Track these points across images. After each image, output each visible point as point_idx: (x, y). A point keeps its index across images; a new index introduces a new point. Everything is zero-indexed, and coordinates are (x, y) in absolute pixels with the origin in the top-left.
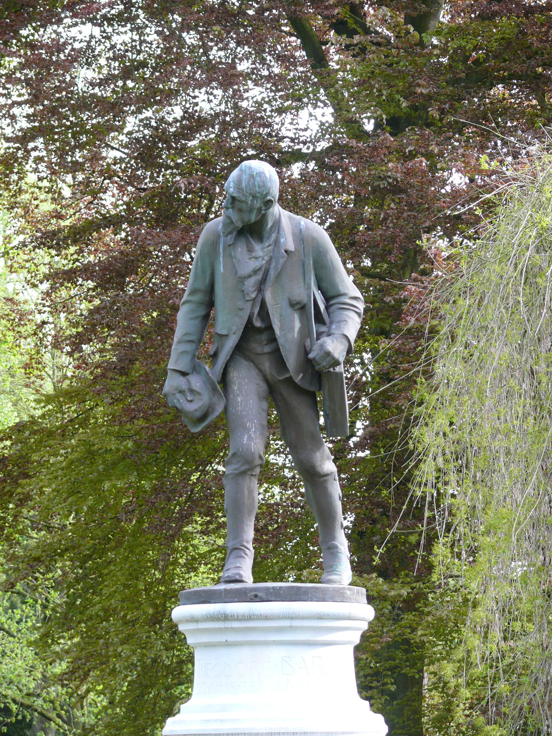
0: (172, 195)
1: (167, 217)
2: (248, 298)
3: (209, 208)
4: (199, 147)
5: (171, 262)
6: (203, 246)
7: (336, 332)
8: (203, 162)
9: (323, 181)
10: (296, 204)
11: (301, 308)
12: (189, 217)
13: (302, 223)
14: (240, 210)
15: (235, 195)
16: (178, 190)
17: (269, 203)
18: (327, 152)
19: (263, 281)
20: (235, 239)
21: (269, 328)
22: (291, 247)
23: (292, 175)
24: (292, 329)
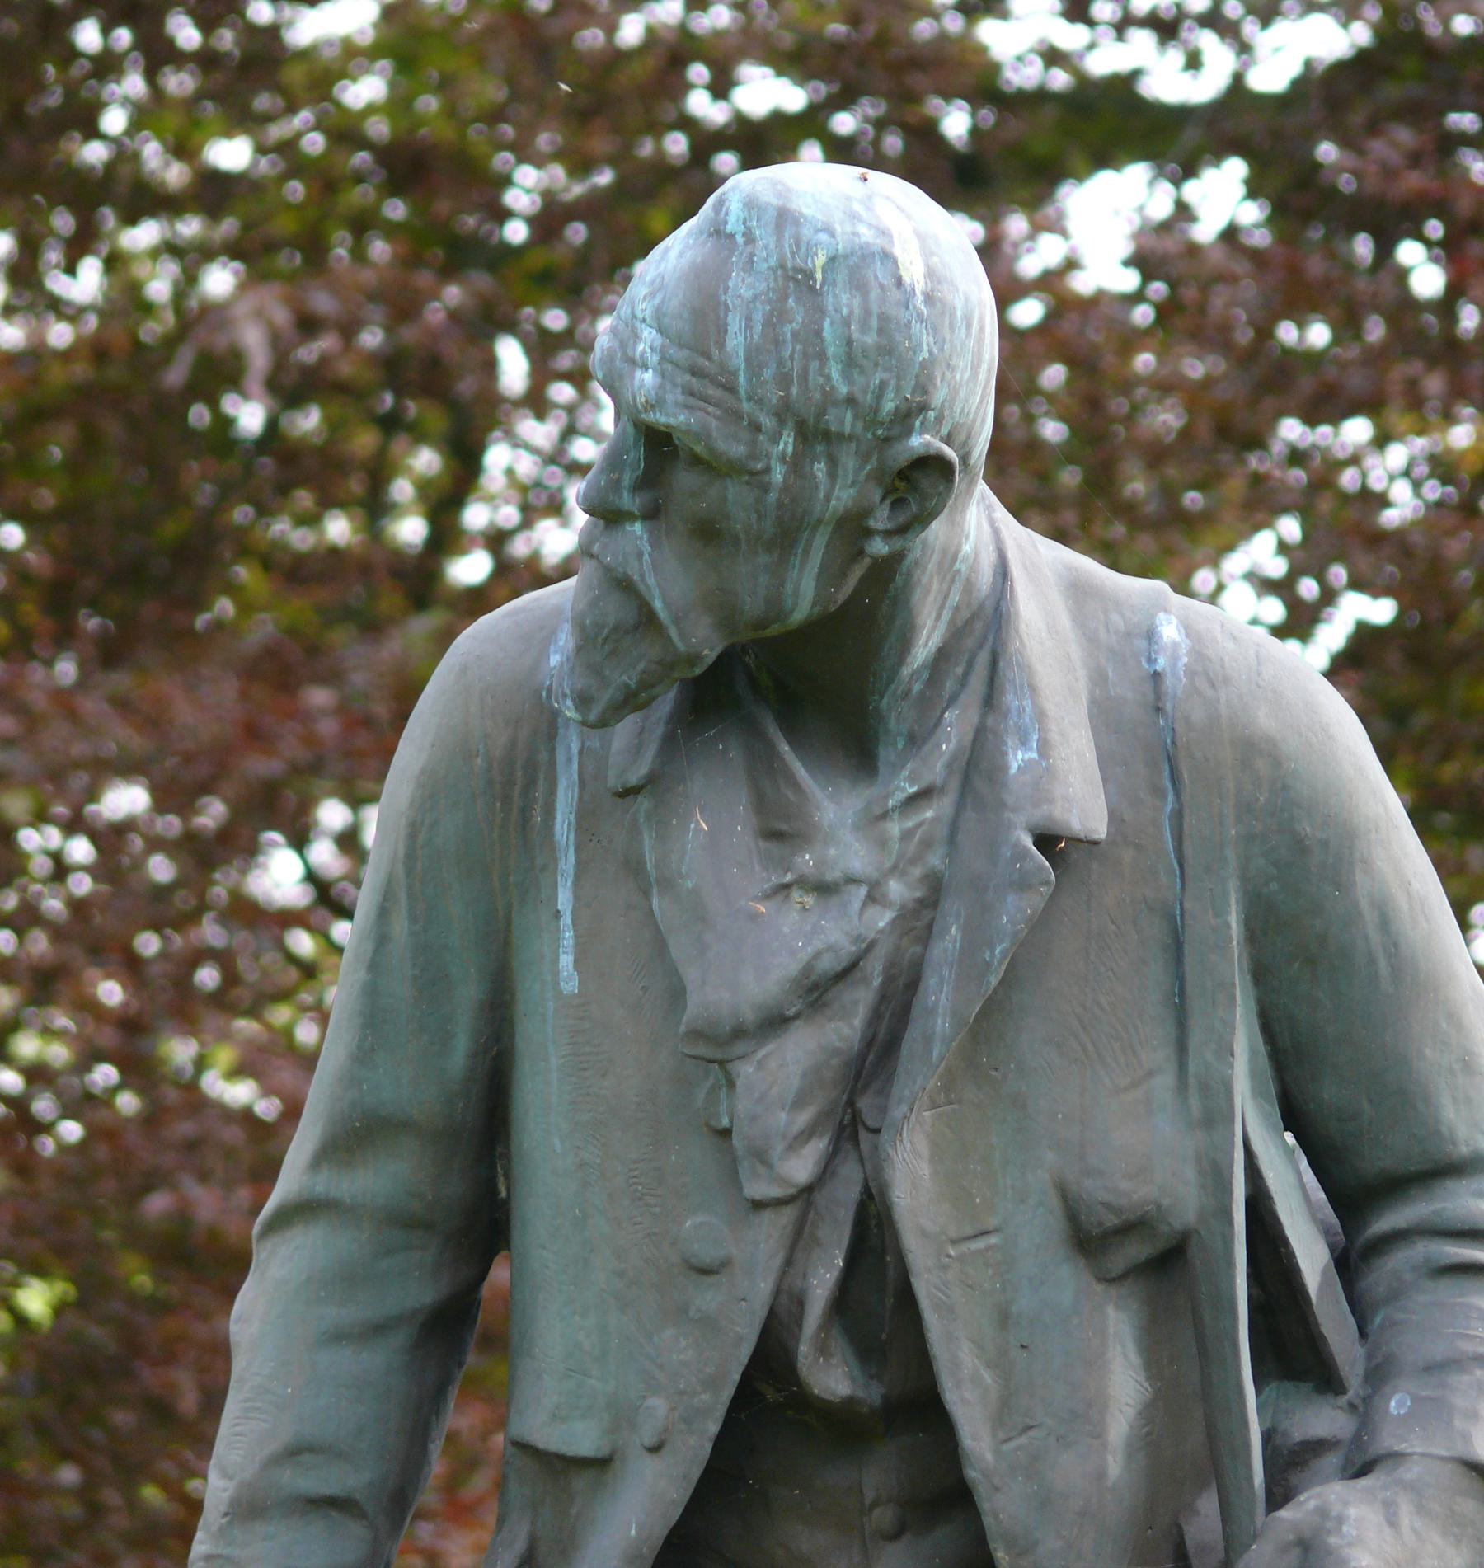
0: (172, 408)
1: (130, 576)
2: (759, 1188)
3: (444, 505)
4: (373, 53)
5: (161, 908)
6: (432, 792)
7: (1413, 1444)
8: (409, 165)
9: (1300, 308)
10: (1102, 480)
11: (1149, 1259)
12: (297, 572)
13: (1169, 631)
14: (708, 533)
15: (674, 417)
16: (220, 373)
17: (921, 484)
18: (1327, 92)
19: (874, 1063)
20: (669, 743)
21: (920, 1410)
22: (1085, 808)
23: (1071, 264)
24: (1086, 1417)
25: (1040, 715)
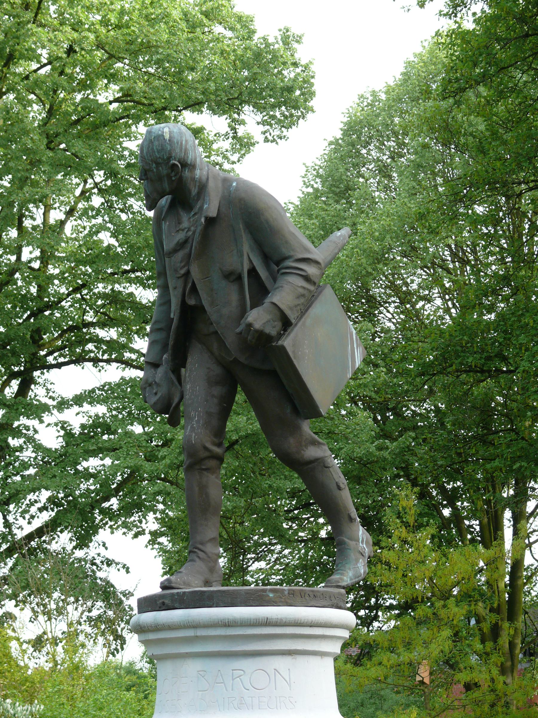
25: (210, 199)
